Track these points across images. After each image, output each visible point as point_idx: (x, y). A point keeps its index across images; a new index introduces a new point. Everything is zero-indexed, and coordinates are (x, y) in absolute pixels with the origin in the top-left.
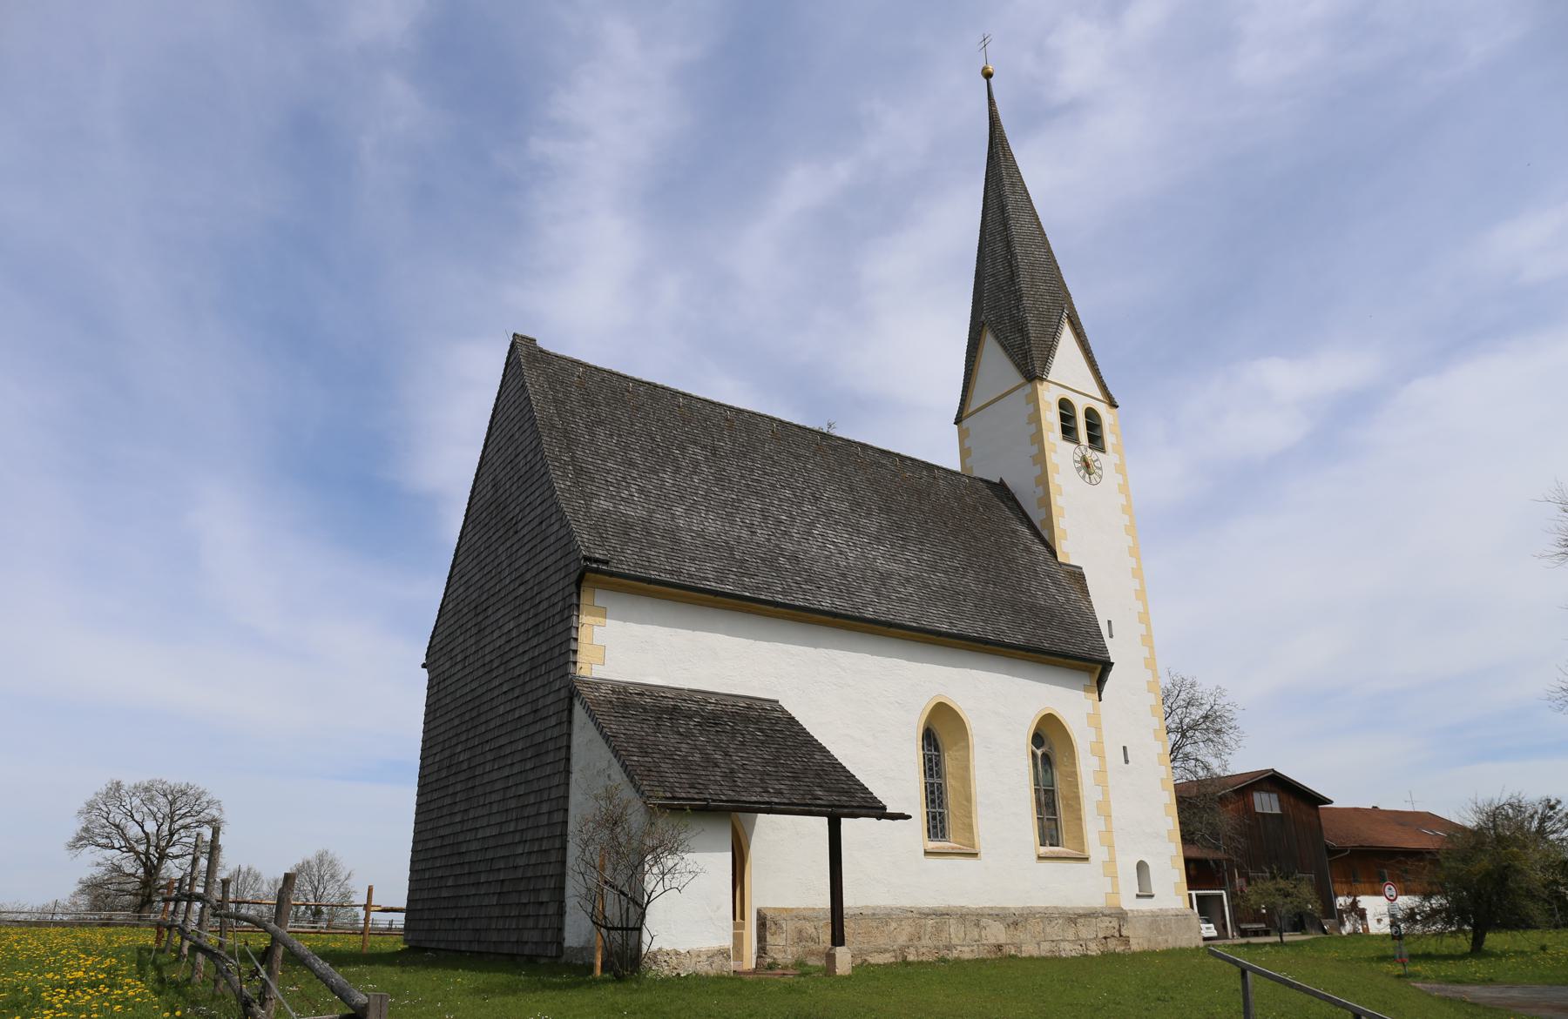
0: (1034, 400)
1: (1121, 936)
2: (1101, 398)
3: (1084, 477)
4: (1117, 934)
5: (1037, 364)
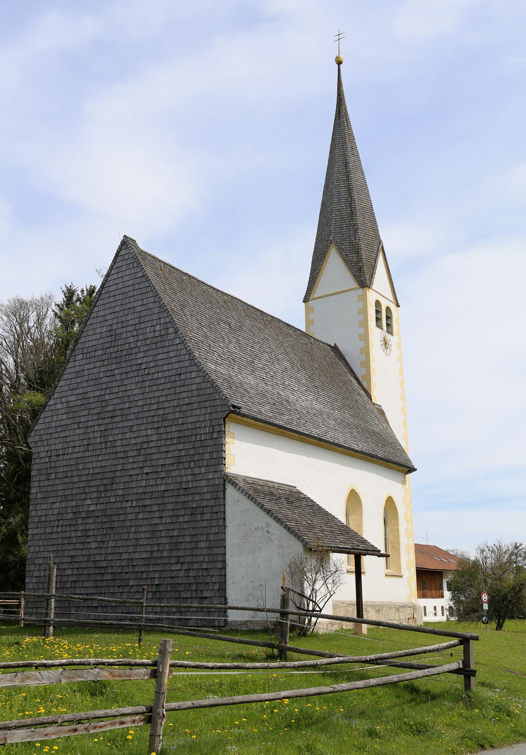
0: (364, 299)
1: (414, 618)
2: (392, 300)
3: (384, 351)
4: (412, 618)
5: (367, 277)
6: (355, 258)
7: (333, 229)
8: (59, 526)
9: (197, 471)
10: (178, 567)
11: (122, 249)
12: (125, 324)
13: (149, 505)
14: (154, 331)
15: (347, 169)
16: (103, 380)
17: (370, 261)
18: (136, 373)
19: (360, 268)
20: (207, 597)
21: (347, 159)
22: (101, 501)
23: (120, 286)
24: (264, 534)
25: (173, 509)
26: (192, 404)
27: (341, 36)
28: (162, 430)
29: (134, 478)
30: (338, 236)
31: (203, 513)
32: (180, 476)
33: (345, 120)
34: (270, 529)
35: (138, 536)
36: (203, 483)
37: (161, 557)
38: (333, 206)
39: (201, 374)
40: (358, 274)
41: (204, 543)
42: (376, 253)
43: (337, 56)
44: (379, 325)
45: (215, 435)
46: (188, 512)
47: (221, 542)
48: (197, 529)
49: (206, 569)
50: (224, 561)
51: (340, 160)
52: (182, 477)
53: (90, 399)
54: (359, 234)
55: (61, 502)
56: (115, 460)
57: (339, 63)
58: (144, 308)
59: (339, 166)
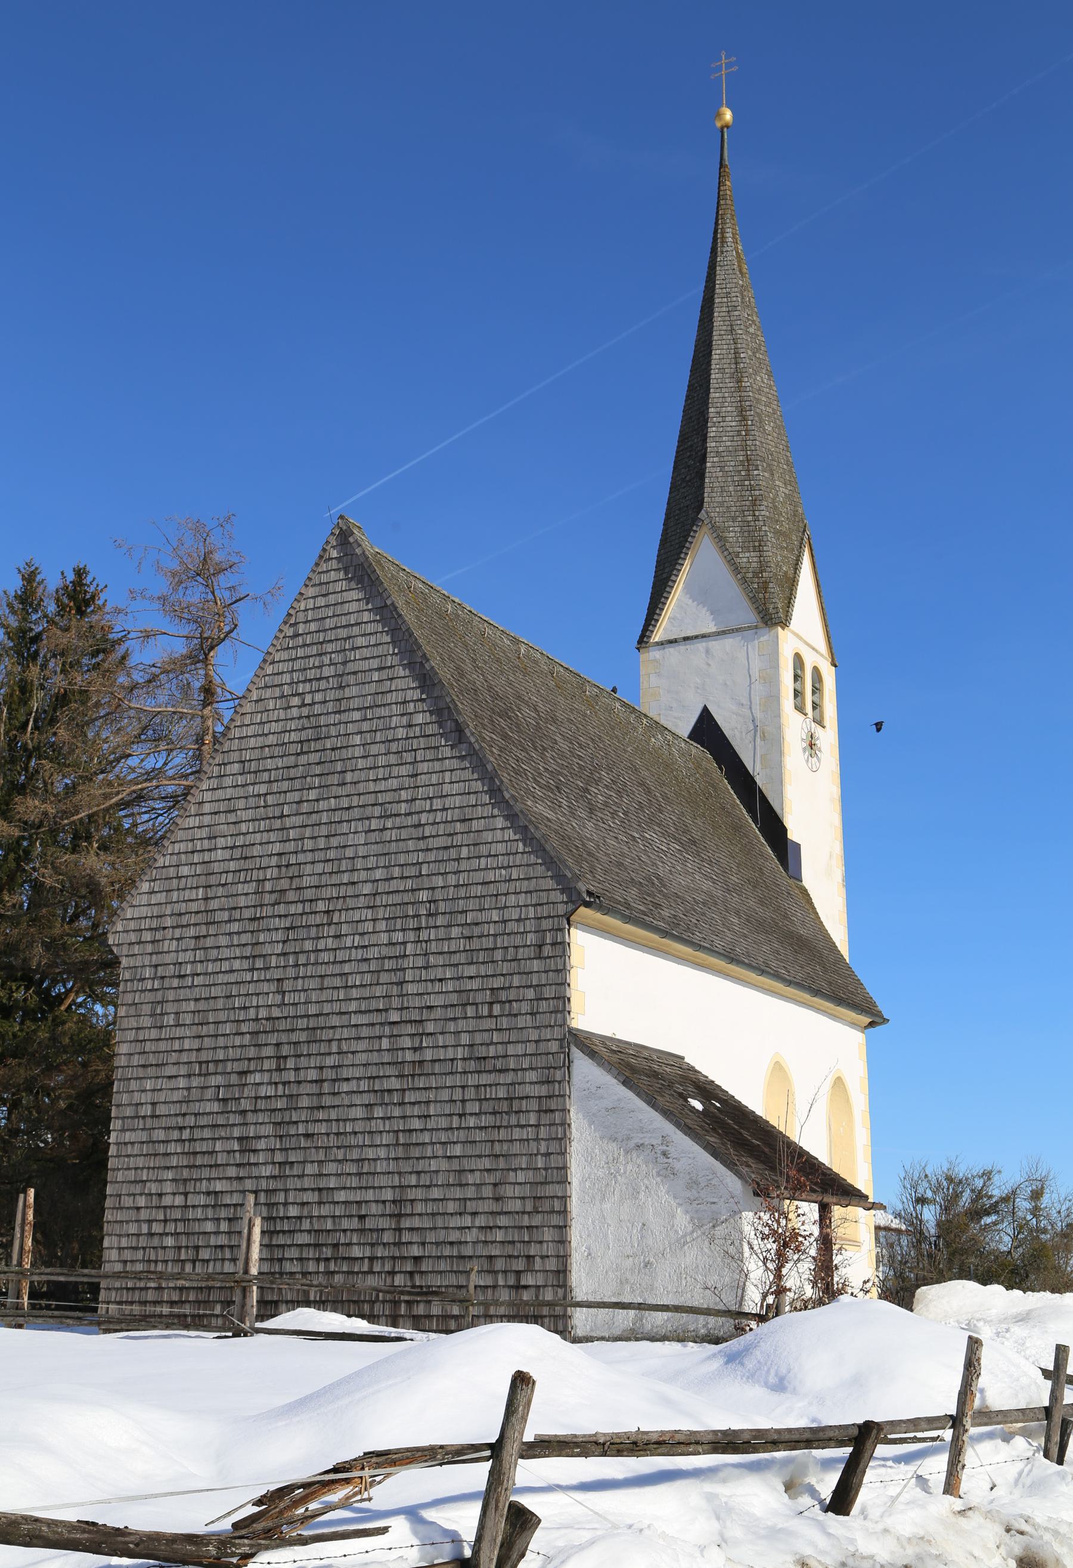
44: (800, 708)
45: (547, 950)
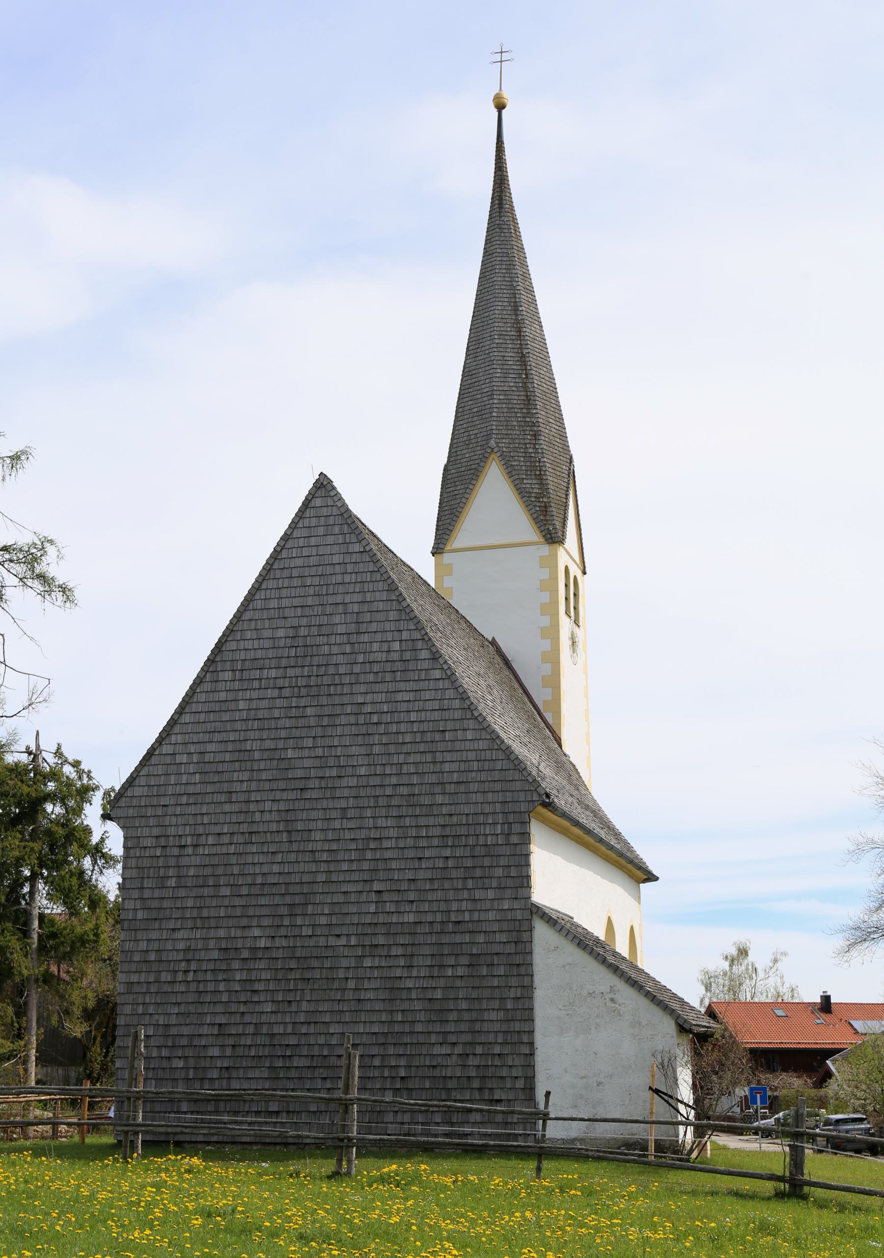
5: (558, 525)
6: (536, 486)
7: (494, 427)
8: (189, 971)
9: (478, 894)
10: (445, 1050)
11: (317, 495)
12: (324, 630)
13: (383, 945)
14: (389, 651)
15: (517, 315)
16: (281, 723)
17: (559, 494)
18: (352, 719)
19: (546, 506)
20: (502, 1100)
21: (517, 296)
22: (283, 932)
23: (313, 561)
24: (606, 1003)
25: (433, 955)
26: (467, 784)
27: (505, 56)
28: (407, 822)
29: (353, 897)
30: (504, 441)
31: (493, 965)
32: (446, 900)
33: (511, 219)
34: (617, 997)
35: (362, 995)
36: (491, 916)
37: (410, 1032)
38: (494, 383)
39: (485, 735)
40: (542, 517)
41: (495, 1012)
42: (566, 480)
43: (497, 95)
45: (515, 839)
46: (465, 960)
47: (527, 1012)
48: (480, 989)
49: (499, 1055)
50: (532, 1044)
51: (505, 296)
52: (450, 902)
53: (252, 753)
54: (541, 442)
55: (192, 929)
56: (311, 864)
57: (500, 107)
58: (365, 608)
59: (503, 308)
